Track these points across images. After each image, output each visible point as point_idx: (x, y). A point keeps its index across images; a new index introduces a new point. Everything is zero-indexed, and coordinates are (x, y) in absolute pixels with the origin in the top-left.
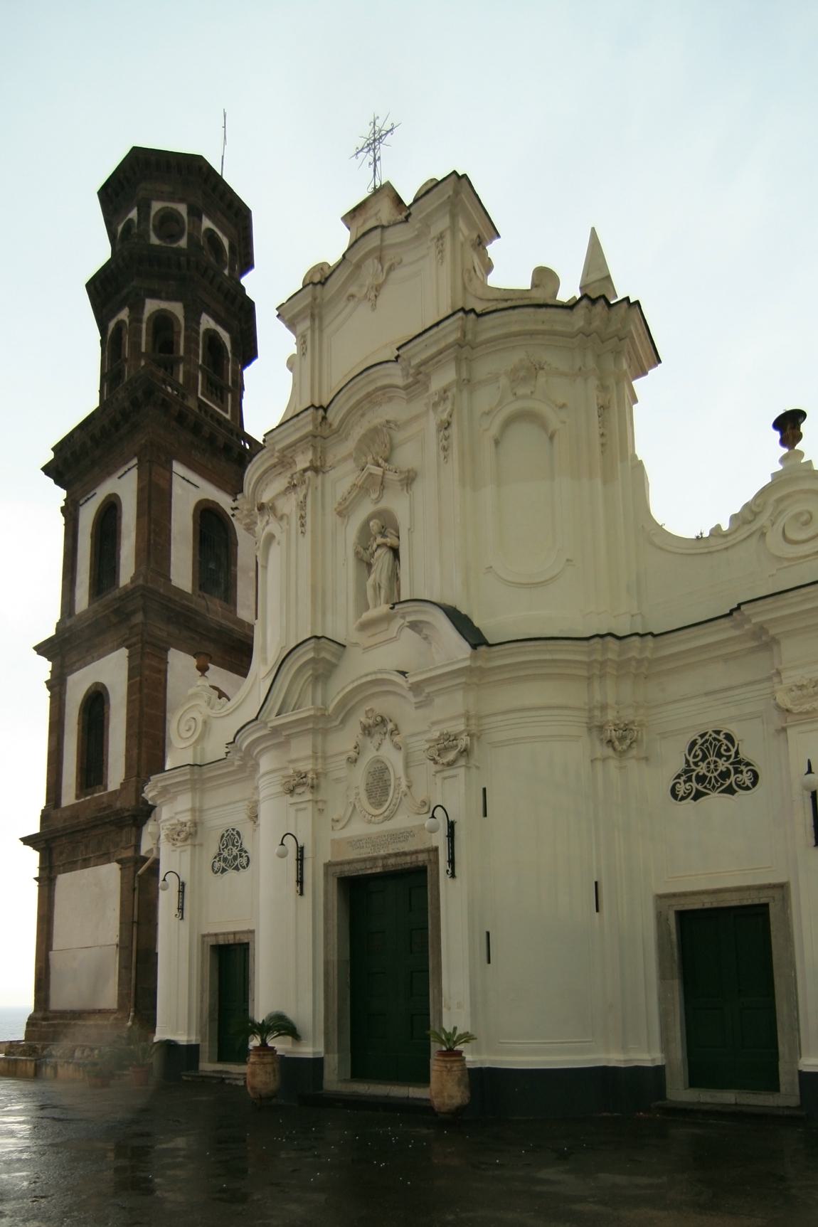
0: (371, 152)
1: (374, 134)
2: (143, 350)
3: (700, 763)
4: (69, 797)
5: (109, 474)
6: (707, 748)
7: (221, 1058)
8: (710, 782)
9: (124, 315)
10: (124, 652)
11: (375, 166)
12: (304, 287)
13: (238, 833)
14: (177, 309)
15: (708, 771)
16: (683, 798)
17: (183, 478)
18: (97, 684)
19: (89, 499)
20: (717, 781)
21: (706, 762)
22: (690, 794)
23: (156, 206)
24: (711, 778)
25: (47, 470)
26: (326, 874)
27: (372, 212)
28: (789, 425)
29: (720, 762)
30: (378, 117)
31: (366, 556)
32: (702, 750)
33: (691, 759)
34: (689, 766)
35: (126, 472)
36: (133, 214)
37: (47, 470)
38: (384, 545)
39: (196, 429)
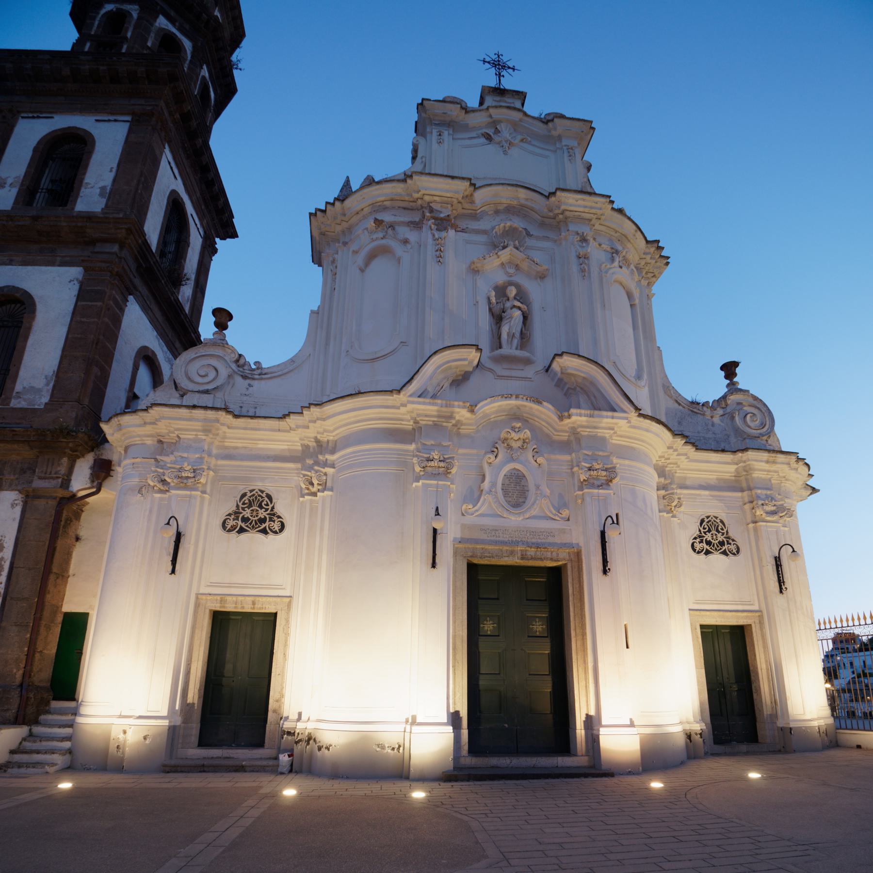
3: (707, 533)
7: (203, 743)
8: (250, 524)
16: (229, 531)
20: (256, 524)
22: (703, 550)
24: (252, 521)
28: (730, 369)
29: (719, 535)
33: (702, 531)
34: (701, 533)
35: (109, 121)
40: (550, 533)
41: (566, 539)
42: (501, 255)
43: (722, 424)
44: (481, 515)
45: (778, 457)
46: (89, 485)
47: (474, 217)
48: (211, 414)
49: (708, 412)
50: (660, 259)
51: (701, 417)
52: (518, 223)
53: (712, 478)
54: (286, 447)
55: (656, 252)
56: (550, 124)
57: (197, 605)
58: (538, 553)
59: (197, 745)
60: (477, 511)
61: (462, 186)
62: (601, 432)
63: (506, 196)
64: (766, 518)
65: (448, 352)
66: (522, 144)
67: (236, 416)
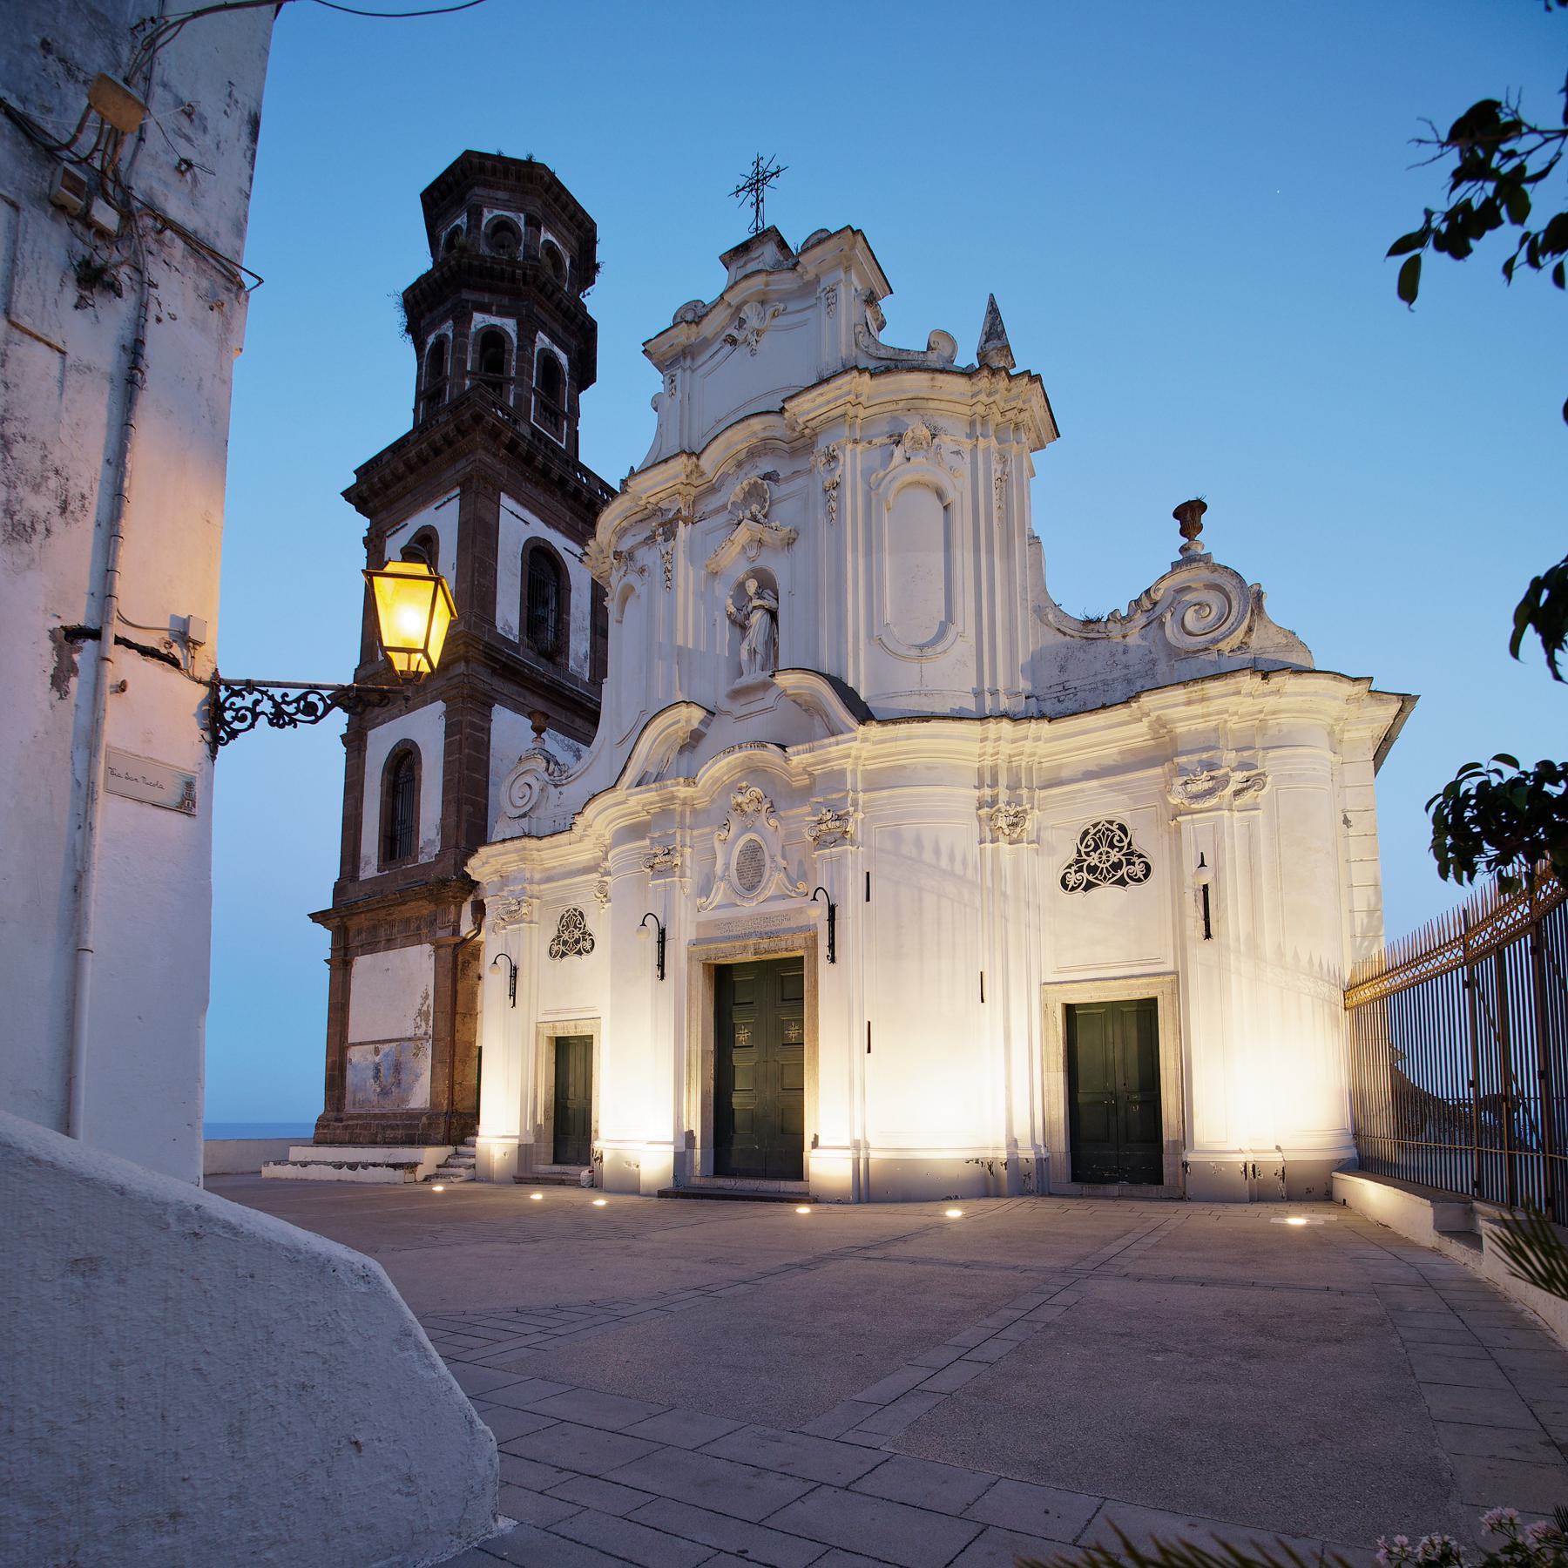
0: (754, 193)
1: (758, 174)
2: (469, 368)
3: (1092, 853)
4: (370, 869)
5: (425, 503)
6: (1100, 838)
7: (556, 1161)
8: (1101, 873)
9: (448, 328)
10: (439, 706)
11: (758, 208)
12: (675, 325)
13: (581, 914)
14: (509, 325)
15: (1100, 862)
16: (1073, 889)
17: (512, 513)
18: (405, 741)
19: (397, 530)
20: (1109, 872)
21: (1098, 852)
23: (487, 215)
25: (347, 494)
26: (690, 959)
27: (754, 254)
28: (1190, 515)
29: (1113, 852)
30: (762, 158)
31: (740, 617)
32: (1094, 840)
33: (1083, 850)
34: (1080, 856)
35: (445, 503)
36: (462, 221)
37: (347, 494)
38: (761, 607)
39: (528, 460)
40: (785, 915)
41: (802, 921)
42: (781, 500)
43: (1144, 643)
44: (718, 907)
45: (1208, 689)
46: (473, 927)
47: (713, 489)
48: (517, 843)
49: (1115, 630)
50: (1013, 383)
51: (1104, 643)
52: (766, 466)
53: (1109, 753)
54: (590, 856)
55: (993, 380)
56: (798, 268)
57: (537, 1033)
58: (772, 944)
59: (551, 1161)
60: (711, 903)
61: (680, 466)
62: (836, 765)
63: (740, 438)
64: (1192, 806)
65: (658, 720)
66: (776, 322)
67: (540, 838)
